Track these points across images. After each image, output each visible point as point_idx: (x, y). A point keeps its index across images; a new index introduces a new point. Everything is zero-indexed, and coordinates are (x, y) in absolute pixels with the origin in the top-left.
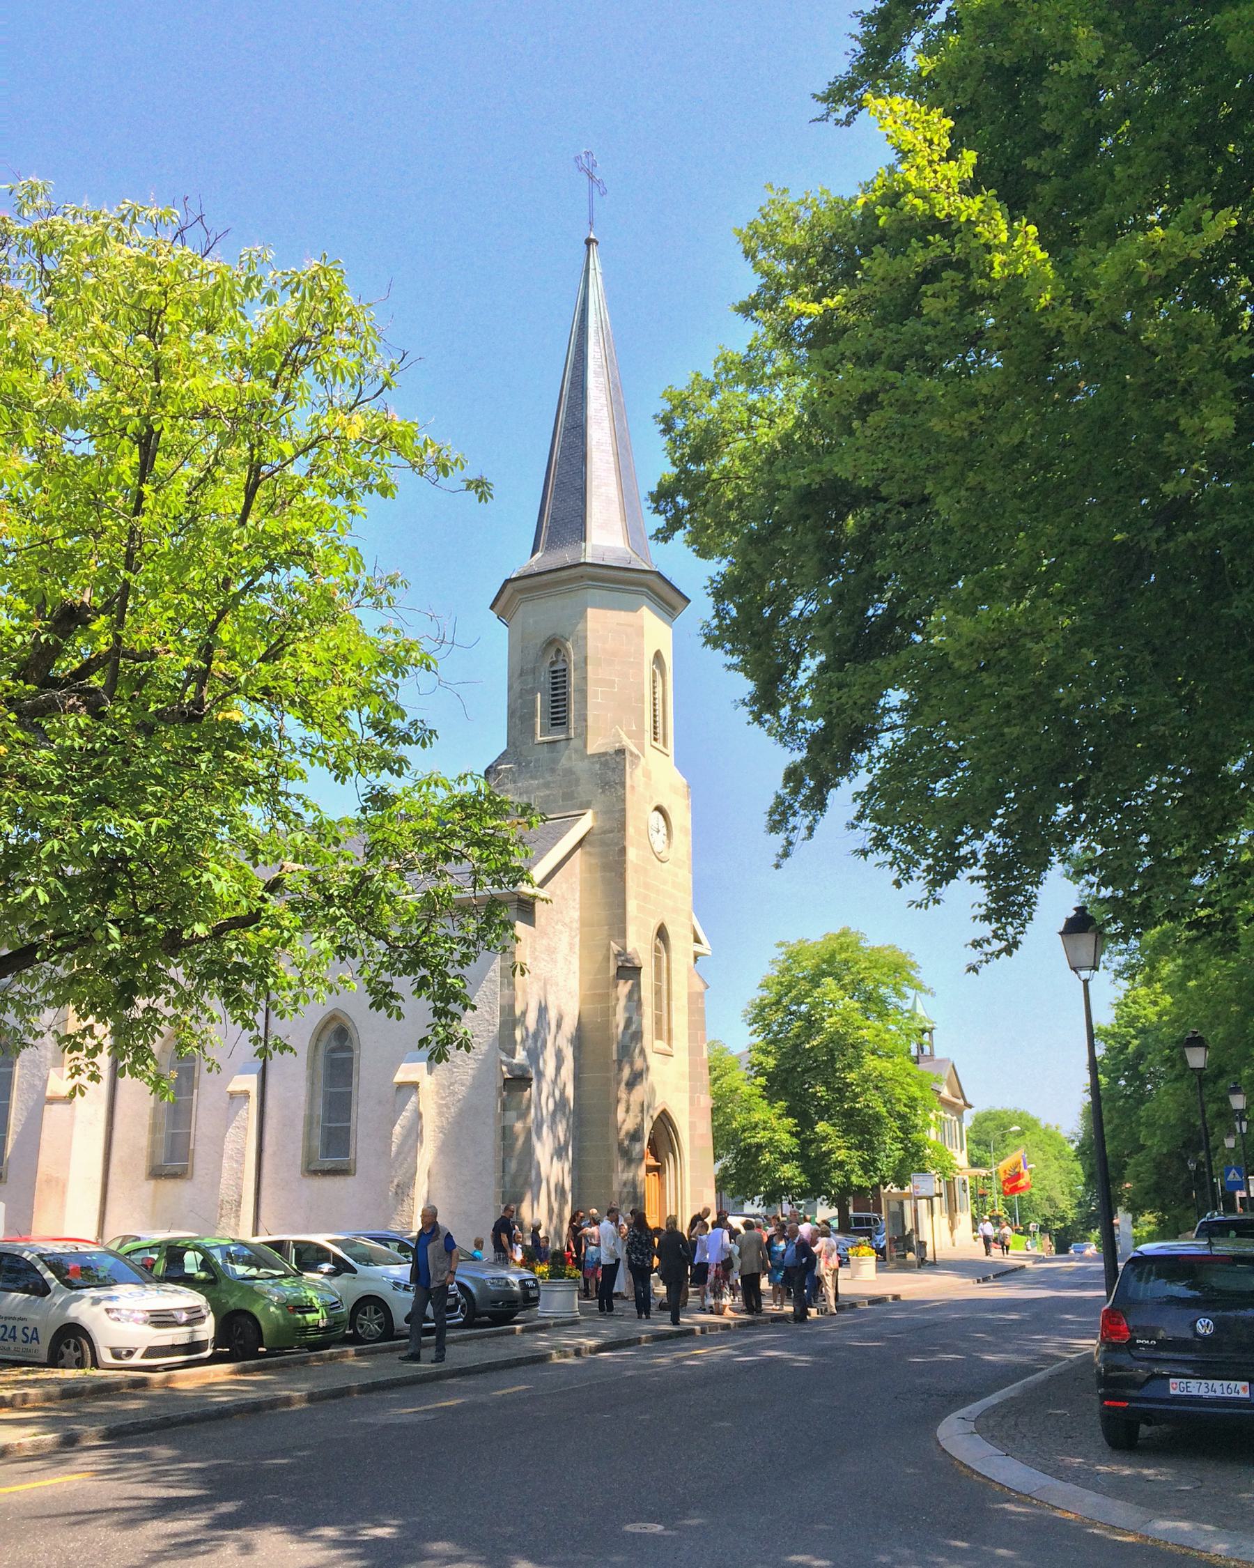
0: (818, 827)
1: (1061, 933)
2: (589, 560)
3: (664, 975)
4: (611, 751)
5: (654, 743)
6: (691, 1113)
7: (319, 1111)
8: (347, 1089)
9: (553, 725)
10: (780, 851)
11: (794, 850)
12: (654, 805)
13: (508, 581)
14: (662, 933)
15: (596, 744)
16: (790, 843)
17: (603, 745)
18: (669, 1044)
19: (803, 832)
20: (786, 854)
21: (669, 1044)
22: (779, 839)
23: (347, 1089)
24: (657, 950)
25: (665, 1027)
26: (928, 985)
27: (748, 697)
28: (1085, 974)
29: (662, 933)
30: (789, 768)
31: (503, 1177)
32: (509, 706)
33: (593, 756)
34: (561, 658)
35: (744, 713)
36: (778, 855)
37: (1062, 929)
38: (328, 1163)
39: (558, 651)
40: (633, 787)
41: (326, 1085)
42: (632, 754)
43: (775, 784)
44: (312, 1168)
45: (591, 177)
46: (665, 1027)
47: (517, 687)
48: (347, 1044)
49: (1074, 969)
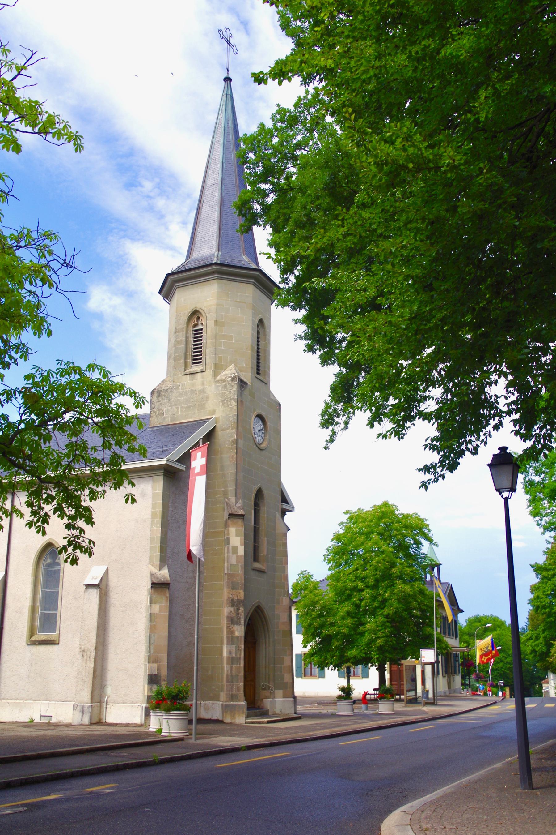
0: (351, 422)
1: (488, 465)
5: (257, 376)
7: (39, 604)
8: (54, 612)
9: (194, 363)
10: (328, 438)
11: (338, 438)
12: (256, 413)
13: (168, 275)
16: (334, 433)
19: (342, 425)
20: (332, 441)
22: (327, 432)
23: (54, 612)
27: (303, 334)
28: (505, 495)
32: (168, 353)
34: (200, 322)
35: (302, 344)
36: (327, 441)
37: (489, 461)
38: (40, 636)
41: (43, 587)
43: (325, 395)
44: (33, 639)
45: (228, 42)
47: (173, 340)
48: (57, 561)
49: (497, 490)
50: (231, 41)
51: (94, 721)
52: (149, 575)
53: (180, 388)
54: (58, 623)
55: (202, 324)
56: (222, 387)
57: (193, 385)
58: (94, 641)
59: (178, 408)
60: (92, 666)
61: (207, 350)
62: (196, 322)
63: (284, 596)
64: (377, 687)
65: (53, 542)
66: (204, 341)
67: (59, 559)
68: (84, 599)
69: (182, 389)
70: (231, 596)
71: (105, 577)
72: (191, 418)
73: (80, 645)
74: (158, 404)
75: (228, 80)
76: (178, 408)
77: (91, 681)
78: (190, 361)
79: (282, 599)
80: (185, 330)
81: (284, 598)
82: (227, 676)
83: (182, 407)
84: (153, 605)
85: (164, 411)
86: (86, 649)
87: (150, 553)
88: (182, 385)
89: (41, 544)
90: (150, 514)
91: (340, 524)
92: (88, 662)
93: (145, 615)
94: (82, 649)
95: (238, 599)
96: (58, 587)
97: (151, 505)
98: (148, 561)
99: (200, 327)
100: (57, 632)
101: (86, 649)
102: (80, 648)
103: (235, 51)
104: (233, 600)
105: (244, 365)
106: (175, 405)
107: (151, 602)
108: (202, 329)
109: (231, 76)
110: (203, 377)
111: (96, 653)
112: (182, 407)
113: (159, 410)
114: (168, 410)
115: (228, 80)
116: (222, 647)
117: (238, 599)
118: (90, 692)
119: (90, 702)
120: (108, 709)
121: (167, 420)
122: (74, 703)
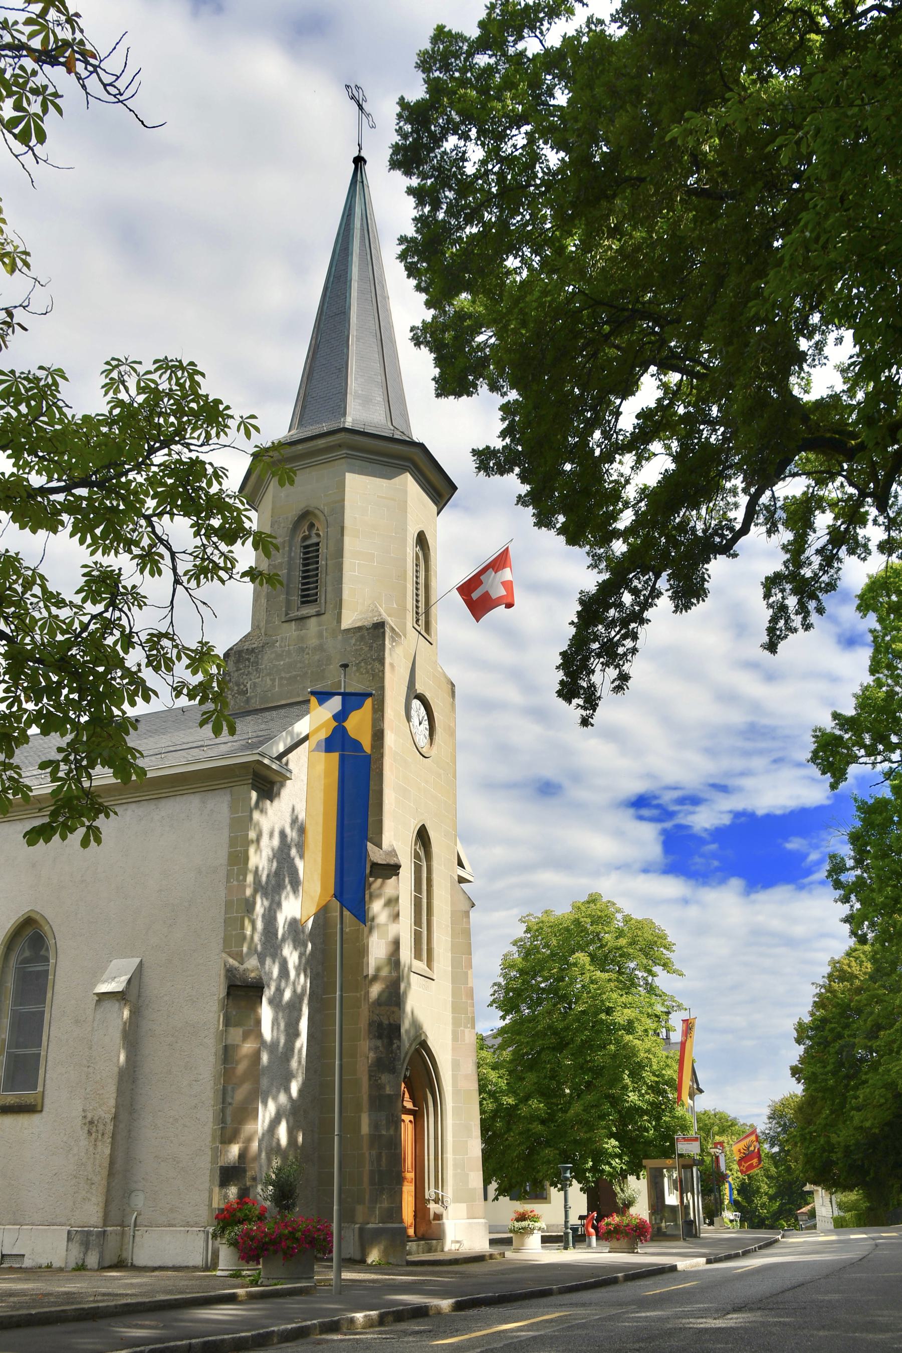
2: (348, 425)
3: (105, 1298)
4: (368, 623)
6: (454, 1049)
8: (34, 1051)
9: (303, 603)
14: (423, 836)
15: (349, 619)
17: (361, 620)
18: (429, 964)
21: (429, 964)
23: (34, 1051)
24: (417, 856)
25: (425, 947)
26: (677, 966)
29: (423, 836)
30: (633, 393)
31: (223, 1110)
33: (347, 631)
34: (314, 531)
39: (312, 526)
40: (392, 665)
41: (15, 1003)
42: (393, 630)
45: (360, 107)
46: (425, 947)
48: (43, 953)
50: (364, 105)
51: (107, 1264)
52: (223, 972)
53: (278, 644)
54: (41, 1072)
55: (318, 535)
56: (356, 640)
57: (302, 639)
58: (112, 1102)
59: (273, 680)
60: (107, 1151)
61: (329, 577)
62: (307, 533)
63: (466, 1027)
64: (585, 1213)
65: (37, 917)
66: (322, 562)
67: (47, 949)
68: (94, 1020)
69: (281, 647)
70: (376, 1018)
71: (137, 979)
72: (299, 696)
73: (84, 1111)
74: (236, 674)
75: (359, 161)
76: (273, 680)
77: (104, 1182)
78: (296, 599)
79: (463, 1032)
80: (287, 545)
81: (467, 1030)
82: (372, 1172)
83: (281, 678)
84: (232, 1030)
85: (248, 685)
86: (96, 1118)
87: (225, 930)
88: (282, 638)
89: (12, 922)
90: (226, 857)
91: (515, 943)
92: (99, 1143)
93: (213, 1050)
94: (89, 1119)
95: (390, 1024)
96: (44, 1003)
97: (227, 840)
98: (221, 946)
99: (314, 540)
100: (40, 1089)
101: (96, 1118)
102: (85, 1117)
103: (371, 123)
104: (380, 1025)
105: (395, 606)
106: (269, 674)
107: (227, 1023)
108: (317, 544)
109: (362, 154)
110: (320, 625)
111: (115, 1126)
112: (281, 678)
113: (238, 685)
114: (255, 684)
115: (359, 161)
116: (360, 1117)
117: (390, 1024)
118: (102, 1205)
119: (101, 1224)
120: (137, 1239)
121: (253, 701)
122: (68, 1228)
